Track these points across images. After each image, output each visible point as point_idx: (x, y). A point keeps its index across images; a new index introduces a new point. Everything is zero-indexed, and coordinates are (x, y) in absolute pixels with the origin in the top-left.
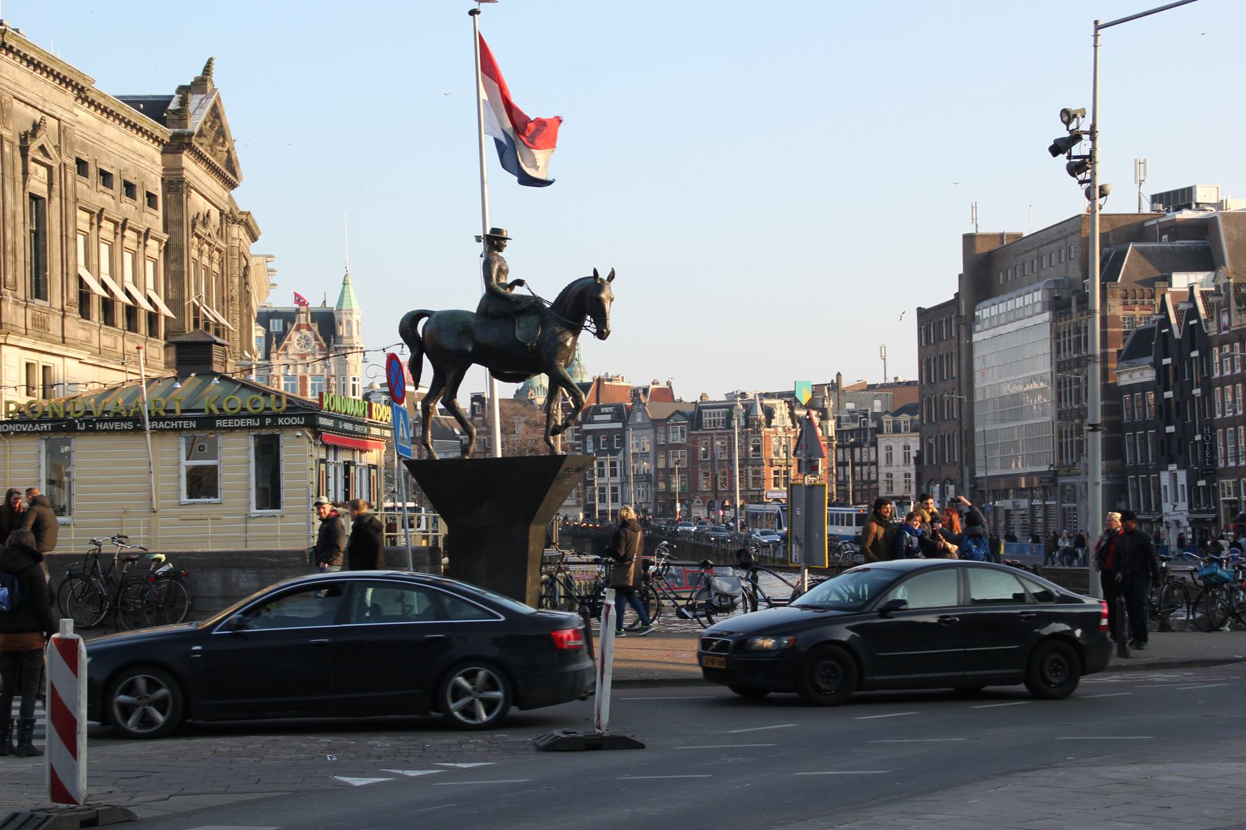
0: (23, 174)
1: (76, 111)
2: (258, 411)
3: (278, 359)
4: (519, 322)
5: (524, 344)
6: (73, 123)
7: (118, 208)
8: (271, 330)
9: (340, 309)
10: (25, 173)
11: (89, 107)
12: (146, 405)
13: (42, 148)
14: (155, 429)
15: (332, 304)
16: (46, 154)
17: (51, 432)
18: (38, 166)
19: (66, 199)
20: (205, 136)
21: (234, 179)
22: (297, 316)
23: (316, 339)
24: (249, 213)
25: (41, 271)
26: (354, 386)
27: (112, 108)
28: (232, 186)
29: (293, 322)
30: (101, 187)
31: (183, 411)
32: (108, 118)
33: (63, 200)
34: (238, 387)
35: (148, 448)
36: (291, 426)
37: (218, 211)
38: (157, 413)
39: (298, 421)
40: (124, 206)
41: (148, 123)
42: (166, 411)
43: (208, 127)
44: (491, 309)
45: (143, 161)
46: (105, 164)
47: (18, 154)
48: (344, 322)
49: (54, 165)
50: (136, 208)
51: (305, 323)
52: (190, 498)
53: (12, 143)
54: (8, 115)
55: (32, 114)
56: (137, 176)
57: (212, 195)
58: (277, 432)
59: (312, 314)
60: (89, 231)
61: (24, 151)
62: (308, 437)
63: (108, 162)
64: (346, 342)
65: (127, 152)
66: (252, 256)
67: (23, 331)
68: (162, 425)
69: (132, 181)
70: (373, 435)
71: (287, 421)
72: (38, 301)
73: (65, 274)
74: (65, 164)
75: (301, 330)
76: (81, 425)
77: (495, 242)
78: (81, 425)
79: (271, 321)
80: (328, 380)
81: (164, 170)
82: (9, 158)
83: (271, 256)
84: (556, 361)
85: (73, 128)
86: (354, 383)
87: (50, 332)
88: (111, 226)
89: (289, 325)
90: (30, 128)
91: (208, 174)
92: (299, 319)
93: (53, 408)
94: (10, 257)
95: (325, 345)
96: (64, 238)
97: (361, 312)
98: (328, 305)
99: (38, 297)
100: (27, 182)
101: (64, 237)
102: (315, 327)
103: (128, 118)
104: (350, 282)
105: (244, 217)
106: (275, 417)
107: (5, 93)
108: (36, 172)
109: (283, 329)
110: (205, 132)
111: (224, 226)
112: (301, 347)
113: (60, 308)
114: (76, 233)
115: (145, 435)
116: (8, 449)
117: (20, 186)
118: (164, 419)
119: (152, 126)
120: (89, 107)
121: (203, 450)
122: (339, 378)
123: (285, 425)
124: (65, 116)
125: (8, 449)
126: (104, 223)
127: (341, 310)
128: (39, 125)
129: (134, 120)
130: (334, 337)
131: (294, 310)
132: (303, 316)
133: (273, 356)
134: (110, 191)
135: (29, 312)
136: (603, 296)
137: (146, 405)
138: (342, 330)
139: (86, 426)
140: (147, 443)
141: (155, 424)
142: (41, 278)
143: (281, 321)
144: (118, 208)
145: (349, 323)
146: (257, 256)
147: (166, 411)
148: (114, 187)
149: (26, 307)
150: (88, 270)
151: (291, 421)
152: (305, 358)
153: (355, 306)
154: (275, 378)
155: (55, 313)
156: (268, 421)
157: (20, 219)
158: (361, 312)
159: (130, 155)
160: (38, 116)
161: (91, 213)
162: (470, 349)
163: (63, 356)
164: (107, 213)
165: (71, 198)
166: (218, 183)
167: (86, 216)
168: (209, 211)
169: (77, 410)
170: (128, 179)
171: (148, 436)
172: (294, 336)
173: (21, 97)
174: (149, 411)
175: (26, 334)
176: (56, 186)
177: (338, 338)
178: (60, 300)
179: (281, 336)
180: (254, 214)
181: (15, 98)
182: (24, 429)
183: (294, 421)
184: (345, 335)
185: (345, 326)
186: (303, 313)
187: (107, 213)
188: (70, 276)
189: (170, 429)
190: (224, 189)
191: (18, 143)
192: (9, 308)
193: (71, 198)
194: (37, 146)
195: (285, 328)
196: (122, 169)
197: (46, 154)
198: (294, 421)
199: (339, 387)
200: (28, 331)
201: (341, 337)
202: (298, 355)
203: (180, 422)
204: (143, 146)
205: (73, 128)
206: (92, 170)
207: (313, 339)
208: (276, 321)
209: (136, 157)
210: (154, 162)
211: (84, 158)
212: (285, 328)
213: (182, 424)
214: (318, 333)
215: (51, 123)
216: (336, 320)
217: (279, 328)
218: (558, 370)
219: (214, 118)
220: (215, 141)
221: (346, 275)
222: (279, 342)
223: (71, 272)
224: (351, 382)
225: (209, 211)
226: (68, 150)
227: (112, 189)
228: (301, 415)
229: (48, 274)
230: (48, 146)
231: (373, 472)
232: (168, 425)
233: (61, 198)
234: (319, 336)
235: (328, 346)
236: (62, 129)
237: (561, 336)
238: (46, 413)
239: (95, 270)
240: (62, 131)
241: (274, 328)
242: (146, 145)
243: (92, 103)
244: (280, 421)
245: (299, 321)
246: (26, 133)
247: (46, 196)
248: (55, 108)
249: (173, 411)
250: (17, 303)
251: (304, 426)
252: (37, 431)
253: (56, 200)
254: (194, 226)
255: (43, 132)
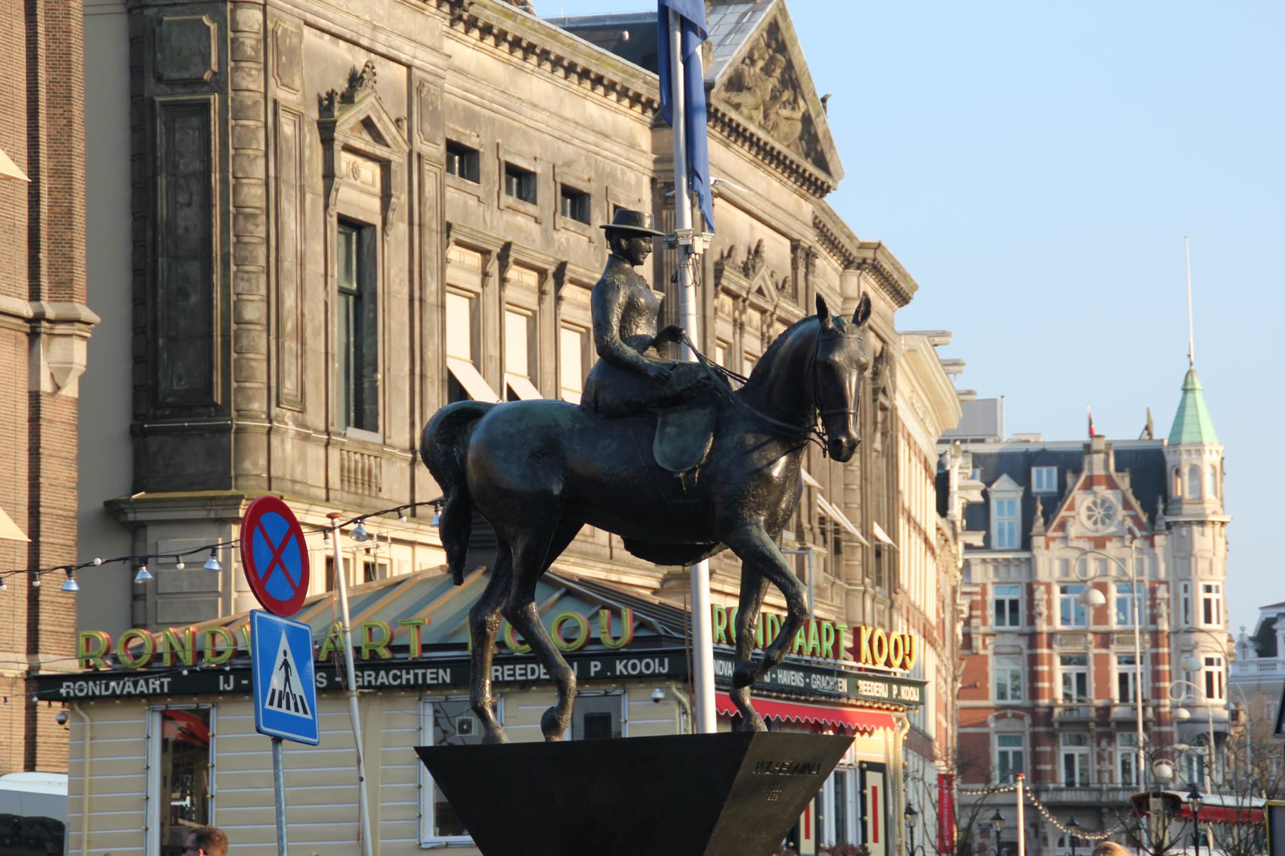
0: (325, 177)
1: (450, 46)
2: (575, 645)
3: (1047, 547)
4: (664, 424)
5: (671, 473)
6: (440, 72)
7: (548, 241)
8: (1035, 489)
9: (1175, 442)
10: (329, 175)
11: (482, 39)
12: (349, 635)
13: (368, 124)
14: (370, 686)
15: (1162, 433)
16: (378, 137)
17: (168, 695)
18: (359, 160)
19: (420, 226)
20: (749, 89)
21: (822, 176)
22: (1087, 459)
23: (1127, 505)
24: (879, 245)
25: (366, 371)
26: (1208, 603)
27: (533, 40)
28: (821, 190)
29: (1077, 471)
30: (512, 200)
31: (426, 648)
32: (525, 59)
33: (416, 228)
34: (557, 595)
35: (353, 729)
36: (641, 678)
37: (788, 242)
38: (373, 653)
39: (655, 666)
40: (561, 236)
41: (616, 67)
42: (392, 648)
43: (758, 69)
44: (608, 397)
45: (607, 145)
46: (519, 154)
47: (312, 138)
48: (1186, 470)
49: (393, 157)
50: (590, 241)
51: (1102, 472)
52: (442, 833)
53: (300, 116)
54: (290, 62)
55: (348, 57)
56: (593, 174)
57: (769, 208)
58: (614, 689)
59: (1118, 454)
60: (479, 290)
61: (327, 130)
62: (680, 703)
63: (526, 148)
64: (1188, 512)
65: (570, 128)
66: (899, 335)
67: (322, 493)
68: (383, 678)
69: (582, 186)
70: (866, 698)
71: (634, 667)
72: (354, 433)
73: (417, 377)
74: (419, 156)
75: (1096, 488)
76: (227, 681)
77: (623, 242)
78: (227, 681)
79: (1034, 470)
80: (1153, 591)
81: (655, 162)
82: (292, 143)
83: (943, 334)
84: (746, 513)
85: (440, 82)
86: (1208, 596)
87: (382, 495)
88: (531, 278)
89: (1070, 478)
90: (341, 85)
91: (758, 166)
92: (1091, 464)
93: (172, 647)
94: (290, 345)
95: (1144, 518)
96: (417, 304)
97: (1221, 448)
98: (1156, 436)
99: (359, 424)
100: (333, 194)
101: (416, 302)
102: (1125, 482)
103: (568, 57)
104: (1198, 385)
105: (869, 254)
106: (610, 657)
107: (285, 16)
108: (355, 172)
109: (1059, 486)
110: (748, 81)
111: (802, 271)
112: (1095, 523)
113: (407, 445)
114: (443, 292)
115: (348, 699)
116: (88, 734)
117: (314, 201)
118: (388, 666)
119: (624, 72)
120: (482, 39)
121: (467, 731)
122: (1175, 587)
123: (630, 677)
124: (422, 59)
125: (88, 734)
126: (513, 273)
127: (1179, 444)
128: (362, 77)
129: (581, 63)
130: (1165, 501)
131: (1080, 447)
132: (1098, 459)
133: (1038, 541)
134: (530, 208)
135: (335, 455)
136: (838, 357)
137: (349, 635)
138: (1181, 487)
139: (237, 682)
140: (351, 719)
141: (369, 676)
142: (366, 385)
143: (1055, 470)
144: (548, 241)
145: (1195, 471)
146: (907, 334)
147: (392, 648)
148: (539, 199)
149: (327, 446)
150: (478, 368)
151: (641, 667)
152: (1104, 546)
153: (1209, 434)
154: (1042, 588)
155: (393, 455)
156: (595, 667)
157: (315, 268)
158: (1221, 448)
159: (579, 133)
160: (359, 59)
161: (485, 253)
162: (557, 490)
163: (412, 544)
164: (519, 252)
165: (433, 224)
166: (785, 185)
167: (475, 259)
168: (760, 242)
169: (219, 648)
170: (572, 182)
171: (355, 700)
172: (1081, 500)
173: (322, 23)
174: (357, 650)
175: (328, 500)
176: (400, 199)
177: (1171, 503)
178: (407, 429)
179: (1054, 503)
180: (891, 247)
181: (307, 24)
182: (113, 684)
183: (648, 666)
184: (1187, 496)
185: (1186, 477)
186: (1098, 452)
187: (519, 252)
188: (428, 383)
189: (401, 687)
190: (802, 196)
191: (314, 114)
192: (288, 447)
193: (433, 224)
194: (353, 121)
195: (1062, 485)
196: (560, 162)
197: (378, 137)
198: (648, 666)
199: (1177, 608)
200: (332, 494)
201: (1180, 501)
202: (1090, 539)
203: (420, 672)
204: (608, 115)
205: (440, 82)
206: (489, 166)
207: (1120, 507)
208: (1044, 470)
209: (591, 137)
210: (633, 145)
211: (471, 141)
212: (1062, 485)
213: (424, 675)
214: (1129, 494)
215: (392, 74)
216: (1169, 465)
217: (1049, 484)
218: (748, 533)
219: (775, 51)
220: (774, 98)
221: (1189, 373)
222: (1049, 515)
223: (433, 373)
224: (1202, 595)
225: (760, 242)
226: (427, 127)
227: (534, 202)
228: (660, 655)
229: (380, 376)
230: (380, 119)
231: (874, 779)
232: (395, 677)
233: (411, 224)
234: (1133, 500)
235: (1152, 520)
236: (416, 84)
237: (756, 455)
238: (158, 657)
239: (493, 367)
240: (414, 87)
241: (1040, 484)
242: (616, 111)
243: (486, 30)
244: (619, 667)
245: (1091, 469)
246: (331, 96)
247: (377, 221)
248: (398, 42)
249: (406, 648)
250: (306, 438)
251: (669, 677)
252: (142, 695)
253: (400, 229)
254: (719, 273)
255: (368, 91)
